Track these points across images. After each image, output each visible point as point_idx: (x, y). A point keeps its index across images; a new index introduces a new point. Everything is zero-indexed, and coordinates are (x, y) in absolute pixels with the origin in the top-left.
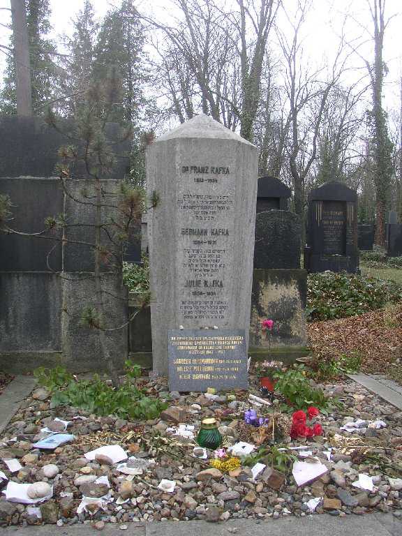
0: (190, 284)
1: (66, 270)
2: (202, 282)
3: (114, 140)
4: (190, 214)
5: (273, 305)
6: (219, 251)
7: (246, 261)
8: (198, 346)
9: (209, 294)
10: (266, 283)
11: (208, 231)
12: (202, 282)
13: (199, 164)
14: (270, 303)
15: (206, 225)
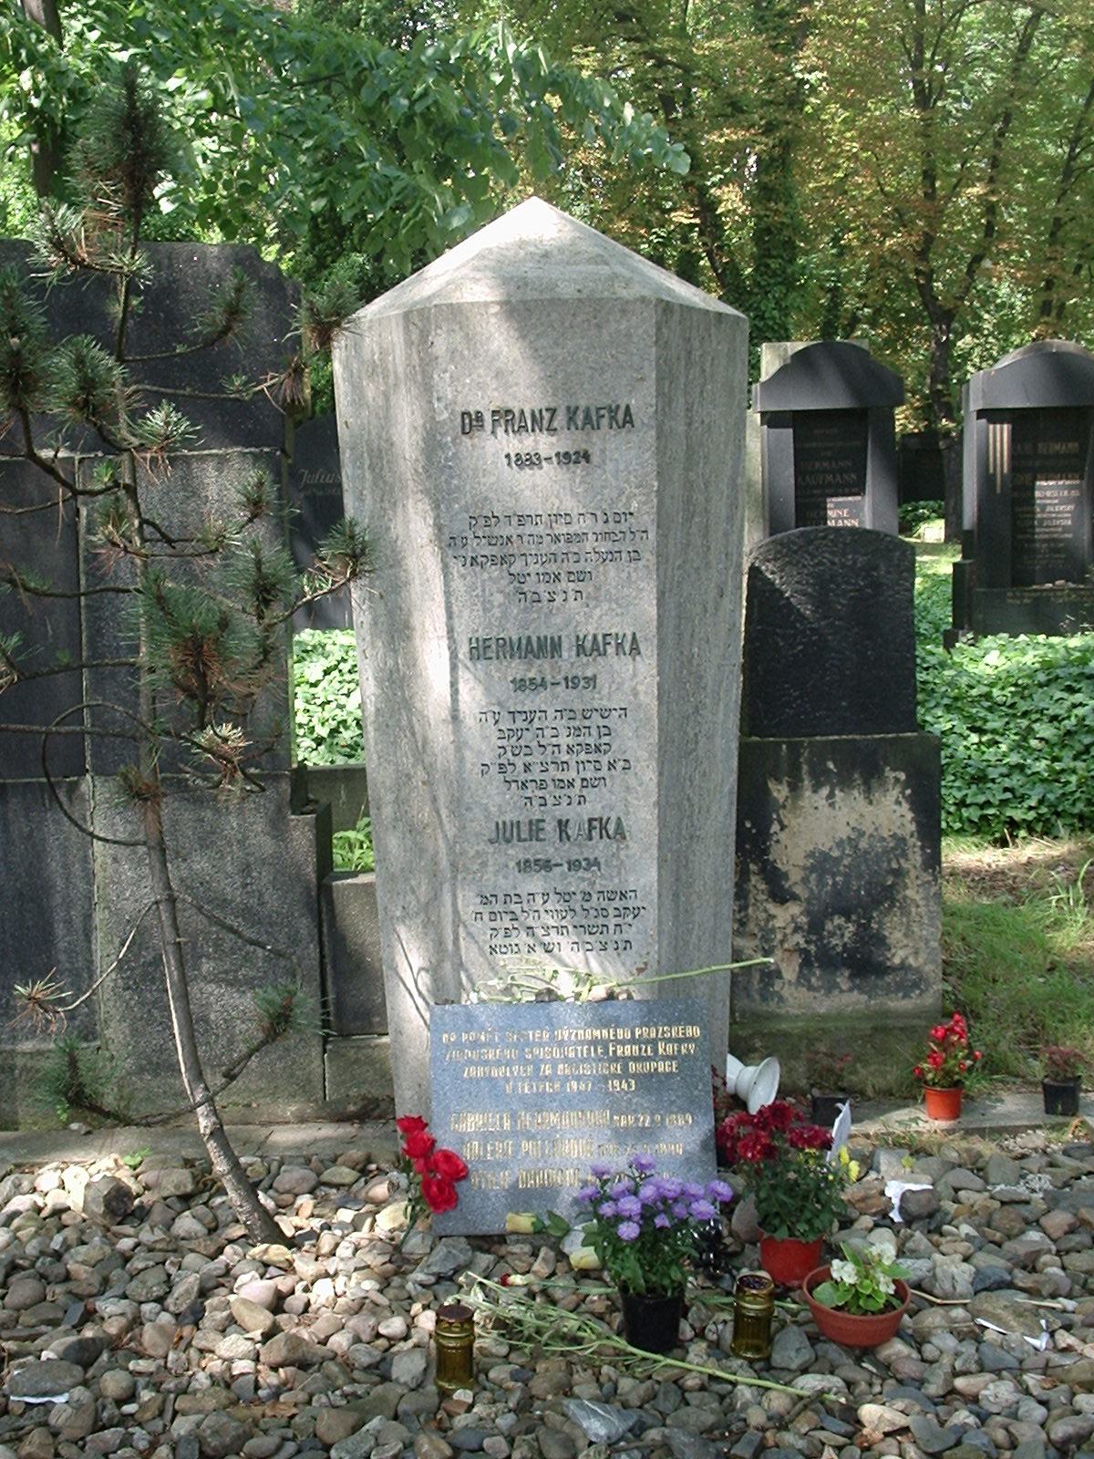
1: (100, 771)
3: (761, 267)
5: (821, 864)
6: (604, 713)
7: (710, 738)
8: (536, 1063)
9: (574, 865)
10: (795, 787)
11: (565, 645)
12: (550, 826)
14: (811, 855)
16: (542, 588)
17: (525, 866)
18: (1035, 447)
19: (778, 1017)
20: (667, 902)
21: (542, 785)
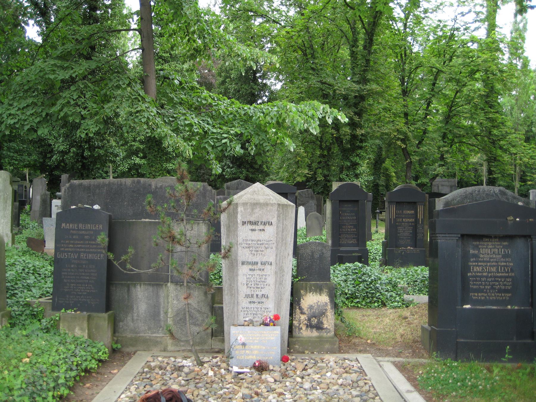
0: (247, 296)
1: (172, 282)
2: (255, 295)
4: (247, 252)
5: (311, 307)
6: (266, 275)
7: (285, 281)
9: (259, 303)
10: (306, 292)
12: (255, 295)
13: (252, 219)
15: (258, 258)
16: (255, 253)
17: (250, 302)
18: (403, 212)
19: (299, 337)
20: (276, 310)
21: (254, 288)
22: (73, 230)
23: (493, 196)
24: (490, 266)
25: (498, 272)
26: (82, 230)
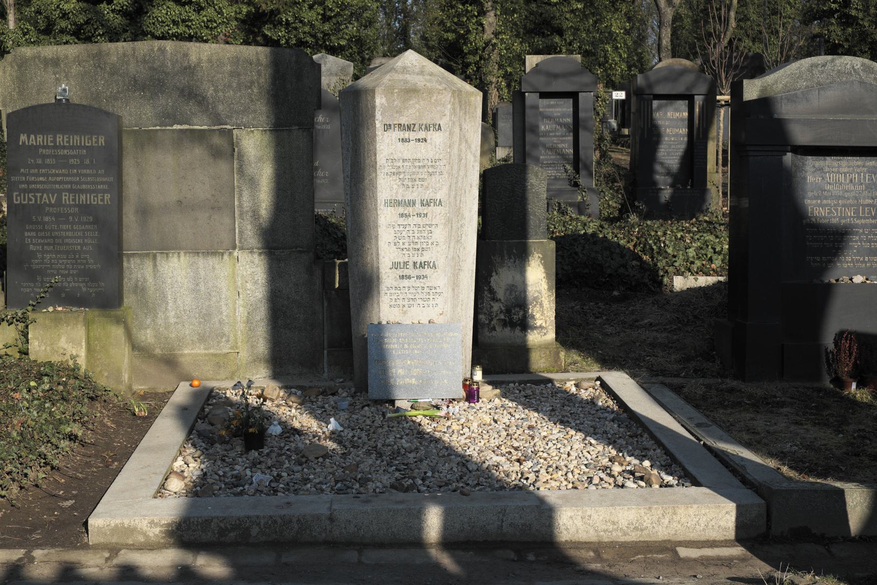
0: (396, 266)
6: (430, 225)
9: (418, 277)
12: (411, 264)
13: (404, 121)
15: (415, 194)
16: (410, 184)
21: (408, 250)
22: (44, 147)
23: (850, 74)
24: (844, 206)
25: (859, 218)
26: (64, 147)
